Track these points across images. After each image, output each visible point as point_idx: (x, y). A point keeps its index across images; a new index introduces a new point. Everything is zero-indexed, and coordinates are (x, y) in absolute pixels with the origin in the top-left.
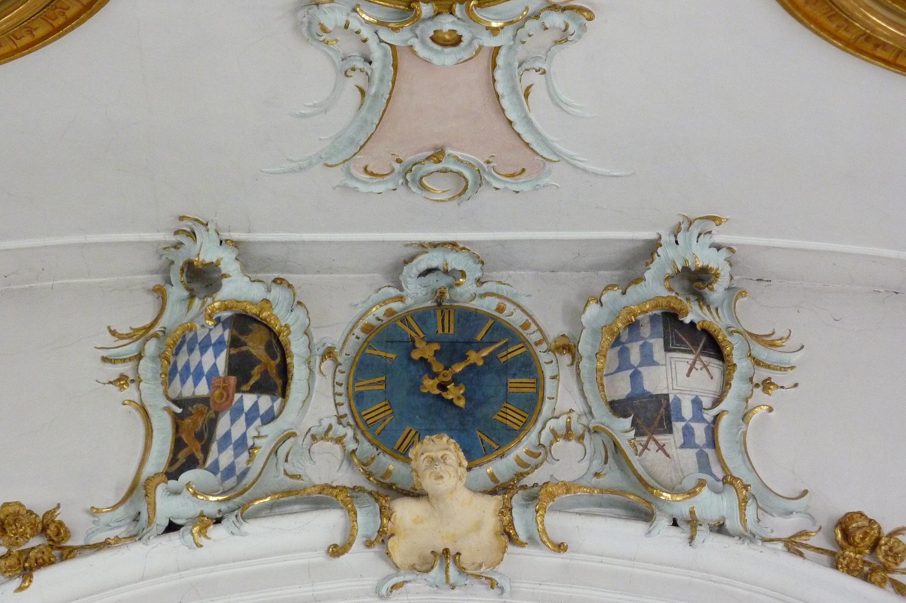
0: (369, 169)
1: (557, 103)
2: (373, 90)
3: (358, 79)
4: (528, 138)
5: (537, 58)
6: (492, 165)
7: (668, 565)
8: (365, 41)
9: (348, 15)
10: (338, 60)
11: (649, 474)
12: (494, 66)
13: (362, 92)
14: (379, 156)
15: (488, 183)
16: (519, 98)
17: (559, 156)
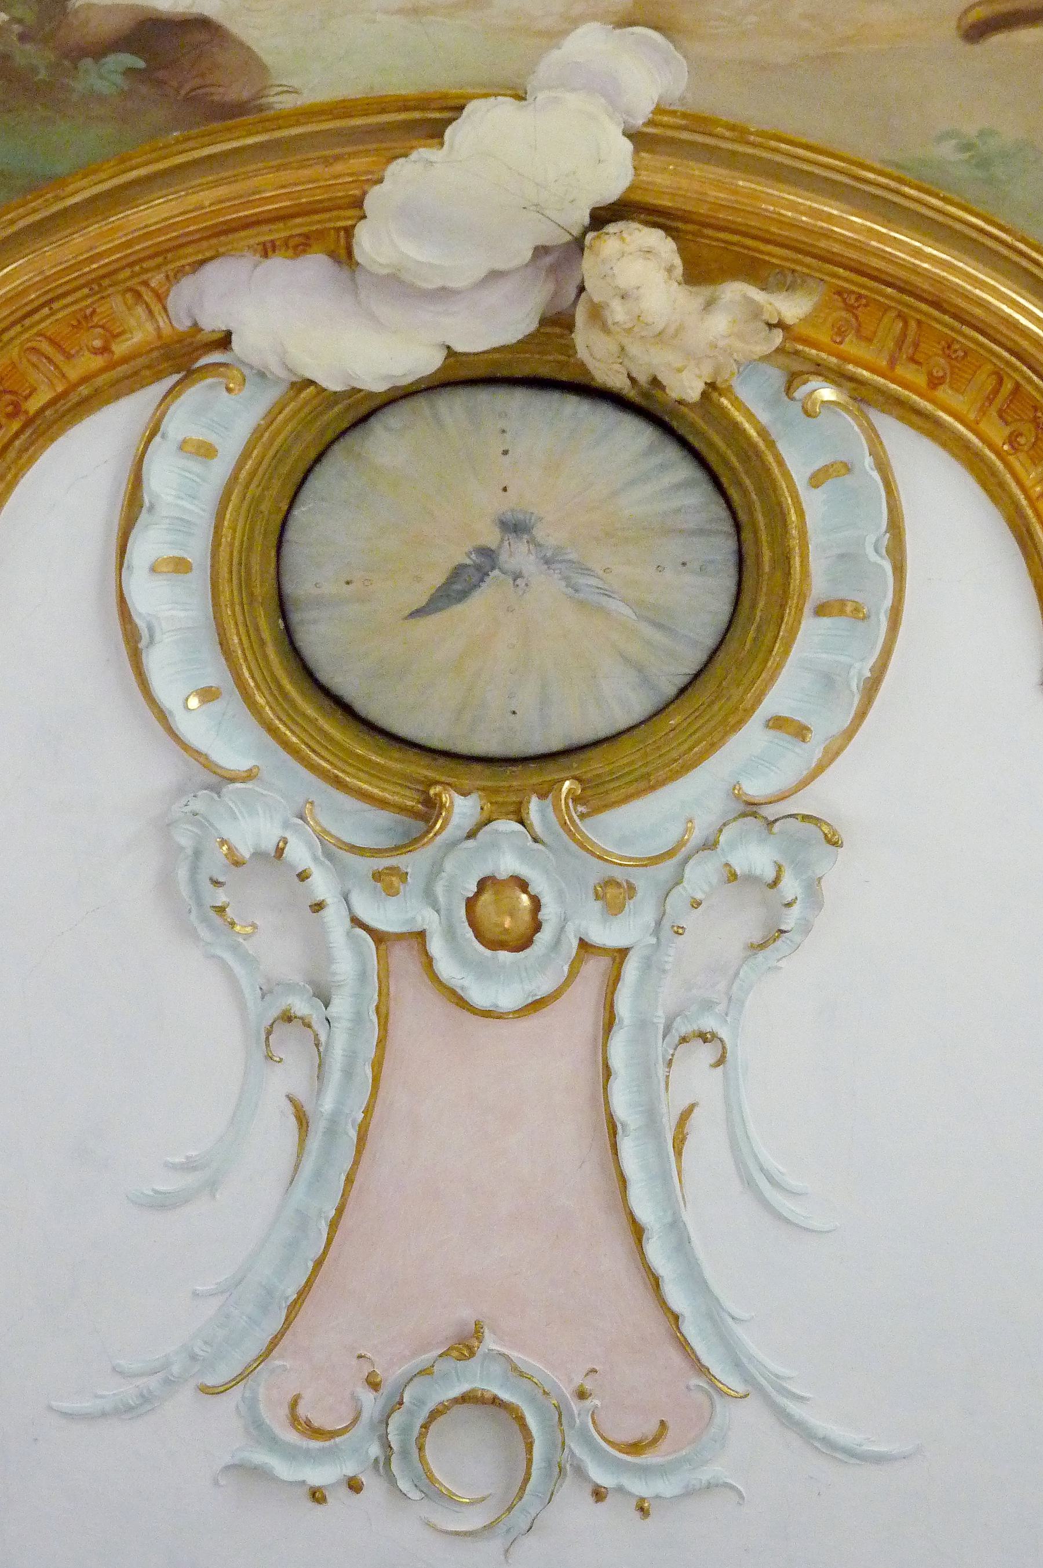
0: (302, 1411)
1: (751, 1177)
2: (328, 1105)
3: (291, 1075)
4: (677, 1298)
5: (708, 1005)
6: (588, 1403)
7: (845, 267)
8: (318, 907)
9: (286, 825)
10: (251, 995)
11: (835, 412)
12: (610, 1022)
13: (302, 1120)
14: (321, 1373)
15: (580, 1471)
16: (661, 1153)
17: (748, 1379)
